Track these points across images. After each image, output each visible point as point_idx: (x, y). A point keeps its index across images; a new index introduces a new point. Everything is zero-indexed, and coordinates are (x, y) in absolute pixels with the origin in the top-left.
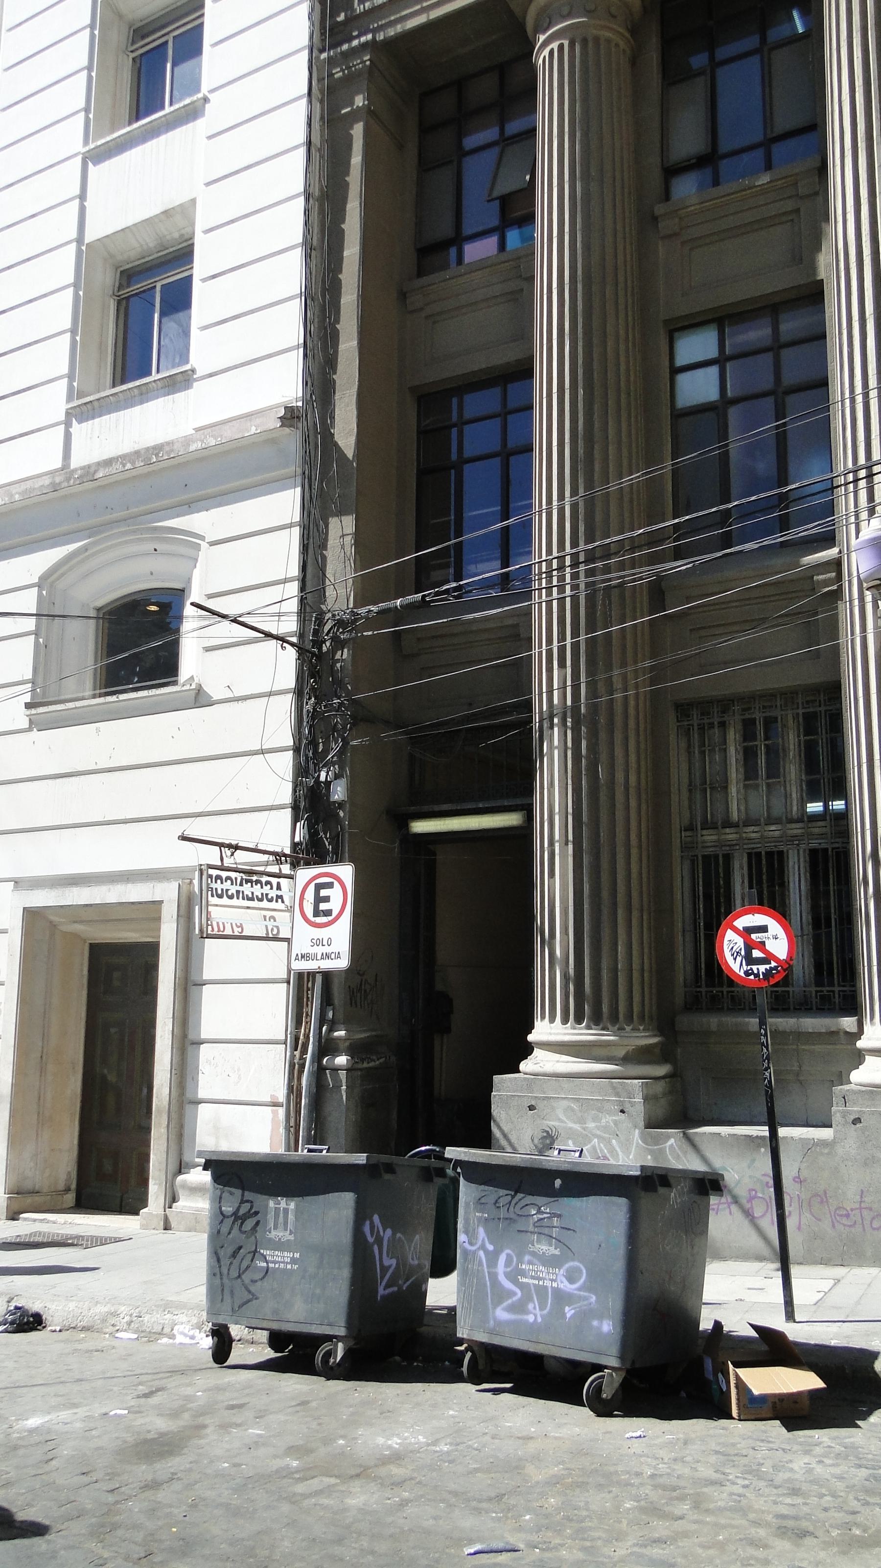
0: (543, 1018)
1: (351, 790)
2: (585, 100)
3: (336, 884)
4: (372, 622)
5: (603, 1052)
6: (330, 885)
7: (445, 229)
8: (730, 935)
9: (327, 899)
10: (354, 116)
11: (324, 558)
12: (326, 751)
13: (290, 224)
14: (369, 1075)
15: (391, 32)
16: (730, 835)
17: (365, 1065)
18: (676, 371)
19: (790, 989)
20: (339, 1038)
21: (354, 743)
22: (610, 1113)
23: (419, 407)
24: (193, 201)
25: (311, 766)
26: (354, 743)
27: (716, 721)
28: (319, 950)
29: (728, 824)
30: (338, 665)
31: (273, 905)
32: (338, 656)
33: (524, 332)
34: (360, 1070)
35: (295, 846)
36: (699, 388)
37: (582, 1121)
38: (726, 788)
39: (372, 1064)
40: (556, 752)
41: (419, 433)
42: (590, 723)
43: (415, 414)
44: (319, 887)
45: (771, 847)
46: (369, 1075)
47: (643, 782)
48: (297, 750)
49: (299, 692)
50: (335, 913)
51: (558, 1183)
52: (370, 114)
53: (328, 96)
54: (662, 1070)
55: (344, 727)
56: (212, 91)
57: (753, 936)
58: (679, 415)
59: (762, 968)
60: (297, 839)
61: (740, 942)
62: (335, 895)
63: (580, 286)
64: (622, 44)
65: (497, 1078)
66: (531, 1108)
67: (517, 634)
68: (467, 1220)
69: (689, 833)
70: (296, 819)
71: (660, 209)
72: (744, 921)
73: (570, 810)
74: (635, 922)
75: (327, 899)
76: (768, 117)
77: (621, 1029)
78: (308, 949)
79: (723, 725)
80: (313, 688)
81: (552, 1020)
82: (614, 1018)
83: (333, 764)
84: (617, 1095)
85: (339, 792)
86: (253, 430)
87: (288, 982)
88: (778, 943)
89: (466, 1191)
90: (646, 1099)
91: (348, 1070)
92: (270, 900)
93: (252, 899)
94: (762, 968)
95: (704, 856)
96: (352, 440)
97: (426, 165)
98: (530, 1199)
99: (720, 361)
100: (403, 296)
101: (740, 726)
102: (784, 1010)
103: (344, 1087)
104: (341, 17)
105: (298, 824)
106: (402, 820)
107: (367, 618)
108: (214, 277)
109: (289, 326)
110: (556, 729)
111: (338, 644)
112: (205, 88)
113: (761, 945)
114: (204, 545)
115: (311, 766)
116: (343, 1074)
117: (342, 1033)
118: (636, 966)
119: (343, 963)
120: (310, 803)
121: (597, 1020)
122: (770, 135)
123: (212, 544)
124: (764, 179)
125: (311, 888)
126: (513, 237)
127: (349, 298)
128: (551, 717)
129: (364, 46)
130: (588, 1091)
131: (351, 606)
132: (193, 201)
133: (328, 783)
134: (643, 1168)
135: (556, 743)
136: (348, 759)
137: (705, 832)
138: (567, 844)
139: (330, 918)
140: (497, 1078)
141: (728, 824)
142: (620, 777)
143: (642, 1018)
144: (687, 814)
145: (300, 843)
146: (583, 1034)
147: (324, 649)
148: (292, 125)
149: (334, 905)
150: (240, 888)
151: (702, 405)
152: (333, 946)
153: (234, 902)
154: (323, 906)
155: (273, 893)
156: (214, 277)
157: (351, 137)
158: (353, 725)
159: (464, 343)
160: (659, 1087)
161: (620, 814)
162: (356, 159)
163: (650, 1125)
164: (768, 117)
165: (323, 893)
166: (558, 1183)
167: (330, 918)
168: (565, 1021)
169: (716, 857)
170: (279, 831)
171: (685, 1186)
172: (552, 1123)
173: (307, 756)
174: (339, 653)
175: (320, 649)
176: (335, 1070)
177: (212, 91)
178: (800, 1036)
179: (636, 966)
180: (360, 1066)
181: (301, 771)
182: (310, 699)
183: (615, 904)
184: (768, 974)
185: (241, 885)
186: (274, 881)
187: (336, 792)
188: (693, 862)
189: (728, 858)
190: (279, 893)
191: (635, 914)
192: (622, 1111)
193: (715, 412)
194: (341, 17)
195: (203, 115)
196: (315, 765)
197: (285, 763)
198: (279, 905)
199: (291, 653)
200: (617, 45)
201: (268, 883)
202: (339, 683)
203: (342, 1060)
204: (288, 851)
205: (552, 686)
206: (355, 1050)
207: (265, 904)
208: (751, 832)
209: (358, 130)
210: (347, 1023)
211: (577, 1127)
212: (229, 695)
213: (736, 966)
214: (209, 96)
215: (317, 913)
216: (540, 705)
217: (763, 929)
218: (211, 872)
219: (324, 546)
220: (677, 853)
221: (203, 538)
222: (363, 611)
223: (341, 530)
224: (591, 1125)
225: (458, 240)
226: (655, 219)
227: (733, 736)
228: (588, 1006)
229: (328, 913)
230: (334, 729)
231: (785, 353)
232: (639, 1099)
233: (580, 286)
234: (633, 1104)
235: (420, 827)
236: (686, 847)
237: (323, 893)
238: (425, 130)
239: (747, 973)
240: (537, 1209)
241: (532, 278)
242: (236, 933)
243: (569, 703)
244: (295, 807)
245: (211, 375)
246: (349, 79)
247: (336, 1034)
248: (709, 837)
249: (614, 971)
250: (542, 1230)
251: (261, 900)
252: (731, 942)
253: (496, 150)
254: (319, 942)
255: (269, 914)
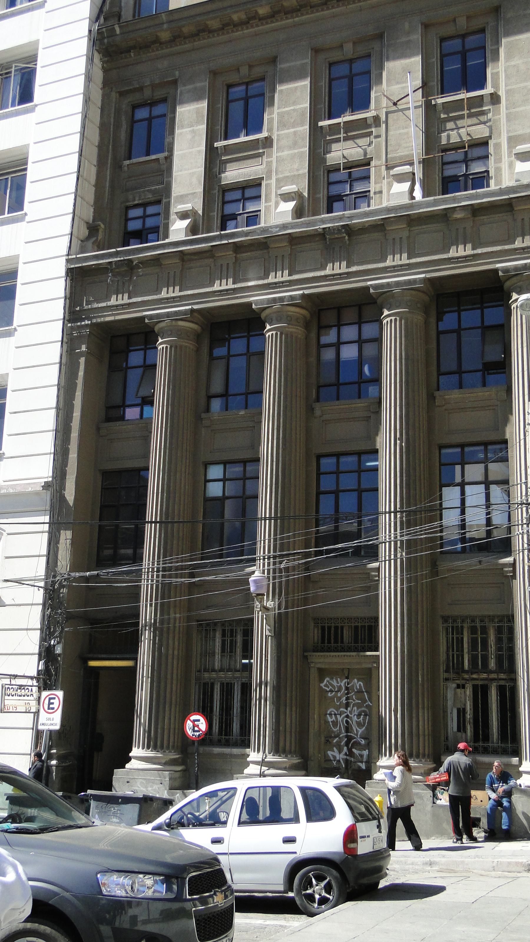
0: (135, 747)
1: (64, 649)
2: (175, 371)
3: (57, 698)
4: (76, 580)
5: (157, 761)
6: (54, 698)
7: (119, 402)
8: (189, 722)
9: (53, 703)
10: (81, 354)
11: (58, 548)
12: (55, 631)
13: (50, 397)
14: (64, 769)
15: (99, 320)
16: (214, 675)
17: (64, 764)
18: (207, 481)
19: (231, 737)
20: (54, 753)
21: (66, 629)
22: (156, 784)
23: (103, 477)
24: (7, 374)
25: (48, 637)
26: (66, 629)
27: (212, 628)
28: (49, 722)
29: (213, 670)
30: (61, 595)
31: (29, 698)
32: (61, 591)
33: (146, 456)
34: (62, 766)
35: (39, 671)
36: (215, 490)
37: (146, 787)
38: (214, 655)
39: (67, 764)
40: (146, 641)
41: (102, 489)
42: (160, 630)
43: (101, 481)
44: (50, 699)
45: (228, 680)
46: (64, 769)
47: (180, 654)
48: (41, 630)
49: (44, 605)
50: (56, 709)
51: (120, 800)
52: (88, 354)
53: (70, 342)
54: (179, 768)
55: (63, 622)
56: (19, 326)
57: (196, 723)
58: (207, 500)
59: (198, 734)
60: (40, 668)
61: (191, 724)
62: (56, 702)
63: (167, 451)
64: (191, 347)
65: (115, 770)
66: (128, 782)
67: (134, 594)
68: (92, 812)
69: (199, 673)
70: (40, 660)
71: (203, 415)
72: (193, 718)
73: (150, 664)
74: (173, 710)
75: (53, 703)
76: (248, 385)
77: (165, 752)
78: (44, 721)
79: (214, 630)
80: (50, 604)
81: (138, 748)
82: (162, 747)
83: (57, 637)
84: (160, 777)
85: (59, 650)
86: (30, 489)
87: (33, 729)
88: (203, 725)
89: (93, 803)
90: (170, 779)
91: (57, 766)
92: (28, 696)
93: (21, 696)
94: (198, 734)
95: (203, 683)
96: (73, 498)
97: (113, 368)
98: (112, 805)
99: (224, 480)
100: (98, 429)
101: (221, 632)
102: (220, 745)
103: (54, 774)
104: (78, 309)
105: (41, 662)
106: (85, 660)
107: (74, 578)
108: (15, 413)
109: (47, 443)
110: (147, 631)
111: (62, 586)
112: (16, 323)
113: (198, 726)
114: (5, 534)
115: (48, 637)
116: (54, 768)
117: (55, 751)
118: (172, 726)
119: (57, 727)
120: (46, 653)
121: (155, 748)
122: (248, 392)
123: (8, 534)
124: (242, 413)
125: (47, 699)
126: (146, 408)
127: (75, 435)
128: (146, 626)
129: (87, 325)
130: (150, 776)
131: (68, 570)
132: (7, 374)
133: (54, 646)
134: (144, 795)
135: (147, 637)
136: (63, 636)
137: (205, 673)
138: (148, 677)
139: (54, 711)
140: (115, 770)
141: (213, 670)
142: (170, 652)
143: (173, 747)
144: (199, 665)
145: (41, 670)
146: (150, 754)
147: (56, 587)
148: (54, 353)
149: (55, 706)
150: (17, 692)
151: (216, 497)
152: (52, 720)
153: (14, 698)
154: (51, 706)
155: (29, 694)
156: (15, 413)
157: (79, 363)
158: (66, 621)
159: (123, 458)
160: (177, 775)
161: (169, 667)
162: (81, 373)
163: (171, 788)
164: (248, 385)
165: (52, 701)
166: (120, 800)
167: (54, 711)
168: (143, 748)
169: (208, 683)
170: (31, 666)
171: (160, 802)
172: (135, 788)
173: (46, 634)
174: (62, 589)
175: (54, 587)
176: (52, 766)
177: (19, 326)
178: (232, 756)
179: (172, 726)
180: (61, 765)
181: (43, 639)
182: (48, 609)
183: (165, 702)
184: (199, 735)
185: (17, 691)
186: (30, 688)
187: (57, 650)
188: (199, 686)
189: (213, 685)
190: (32, 693)
191: (173, 706)
192: (161, 784)
193: (221, 500)
194: (78, 309)
195: (14, 336)
196: (50, 638)
197: (36, 635)
198: (31, 698)
199: (42, 590)
200: (190, 348)
201: (27, 689)
202: (61, 603)
203: (54, 762)
204: (36, 676)
205: (147, 613)
206: (59, 758)
207: (26, 698)
208: (222, 674)
209: (82, 360)
210: (57, 747)
211: (144, 789)
212: (13, 603)
213: (190, 733)
214: (17, 328)
215: (49, 708)
216: (142, 621)
217: (199, 720)
218: (7, 686)
219: (58, 542)
220: (193, 681)
221: (5, 531)
222: (73, 574)
223: (66, 537)
224: (150, 789)
225: (124, 406)
226: (202, 419)
227: (218, 635)
228: (152, 743)
229: (53, 708)
230: (58, 622)
231: (247, 481)
232: (168, 779)
233: (167, 451)
234: (165, 781)
235: (93, 664)
236: (198, 679)
237: (52, 701)
238: (113, 352)
239: (193, 735)
240: (114, 808)
241: (151, 432)
242: (14, 711)
243: (153, 621)
244: (40, 654)
245: (11, 457)
246: (79, 337)
247: (52, 751)
248: (206, 675)
249: (163, 729)
250: (115, 815)
251: (24, 696)
252: (189, 724)
253: (141, 369)
254: (49, 719)
255: (27, 702)
